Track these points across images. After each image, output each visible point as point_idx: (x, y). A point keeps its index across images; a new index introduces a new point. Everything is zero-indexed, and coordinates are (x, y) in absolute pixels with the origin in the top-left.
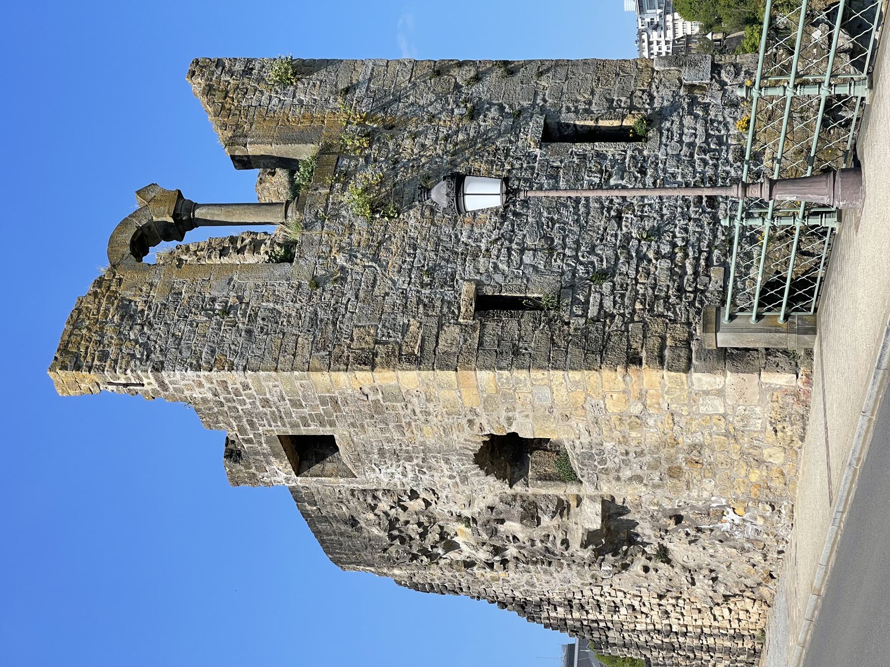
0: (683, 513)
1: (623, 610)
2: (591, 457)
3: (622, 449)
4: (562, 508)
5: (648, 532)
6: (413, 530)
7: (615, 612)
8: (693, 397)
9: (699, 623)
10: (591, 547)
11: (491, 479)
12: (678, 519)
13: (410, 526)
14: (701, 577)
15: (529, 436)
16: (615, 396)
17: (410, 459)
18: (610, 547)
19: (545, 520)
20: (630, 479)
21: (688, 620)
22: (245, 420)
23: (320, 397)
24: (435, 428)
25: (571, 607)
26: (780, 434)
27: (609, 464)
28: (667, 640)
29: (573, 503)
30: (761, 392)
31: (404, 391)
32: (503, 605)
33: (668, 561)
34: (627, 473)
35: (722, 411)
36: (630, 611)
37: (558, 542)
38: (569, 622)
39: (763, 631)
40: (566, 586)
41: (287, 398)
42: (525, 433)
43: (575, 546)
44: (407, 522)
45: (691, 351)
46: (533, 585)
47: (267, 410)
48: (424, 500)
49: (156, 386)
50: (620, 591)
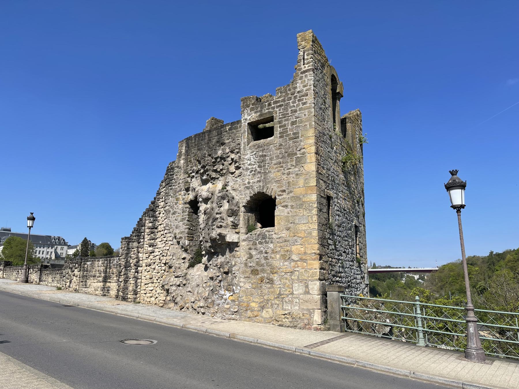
0: (230, 275)
5: (219, 261)
6: (219, 167)
9: (143, 278)
10: (218, 237)
12: (227, 273)
13: (221, 166)
14: (181, 280)
15: (276, 214)
16: (302, 249)
18: (214, 244)
19: (231, 219)
20: (250, 254)
25: (152, 229)
26: (283, 316)
27: (259, 246)
29: (237, 230)
32: (153, 203)
33: (188, 268)
34: (254, 252)
35: (294, 292)
37: (221, 224)
38: (143, 228)
39: (139, 303)
40: (174, 227)
41: (298, 120)
43: (219, 231)
48: (235, 172)
49: (304, 69)
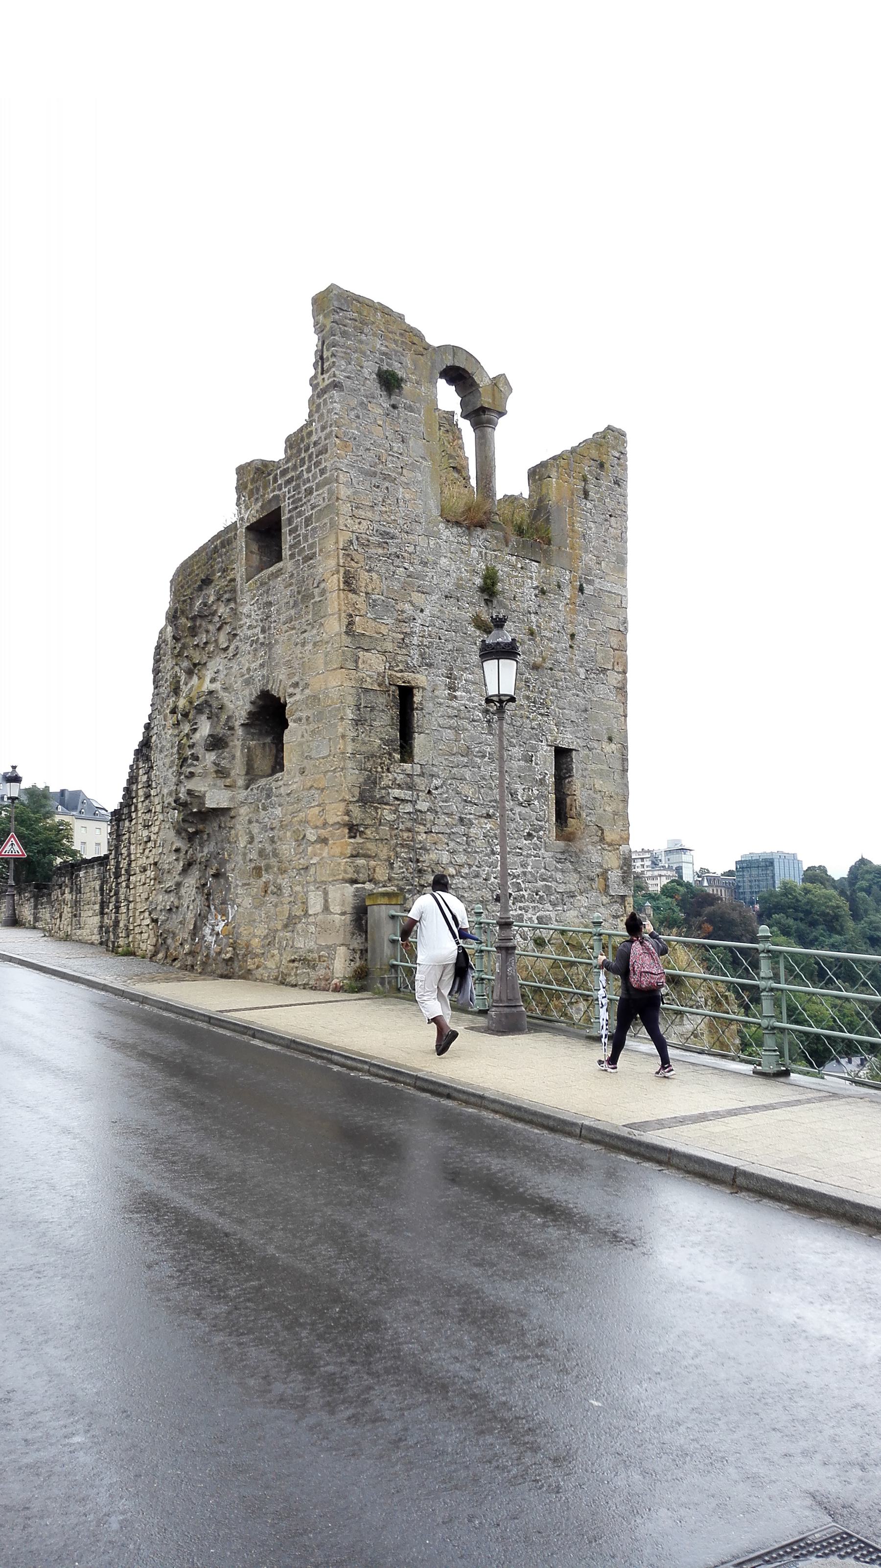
1: (145, 833)
2: (268, 796)
3: (276, 823)
4: (221, 772)
7: (144, 826)
8: (322, 886)
9: (138, 899)
11: (248, 707)
14: (172, 899)
15: (286, 738)
17: (263, 631)
19: (211, 757)
20: (250, 832)
21: (140, 889)
22: (293, 474)
23: (315, 542)
24: (290, 652)
28: (123, 872)
29: (228, 781)
30: (328, 947)
31: (322, 620)
34: (255, 829)
35: (310, 912)
36: (145, 839)
38: (134, 787)
40: (161, 780)
42: (287, 736)
44: (207, 632)
45: (364, 883)
46: (161, 751)
47: (302, 495)
48: (228, 647)
50: (159, 829)
